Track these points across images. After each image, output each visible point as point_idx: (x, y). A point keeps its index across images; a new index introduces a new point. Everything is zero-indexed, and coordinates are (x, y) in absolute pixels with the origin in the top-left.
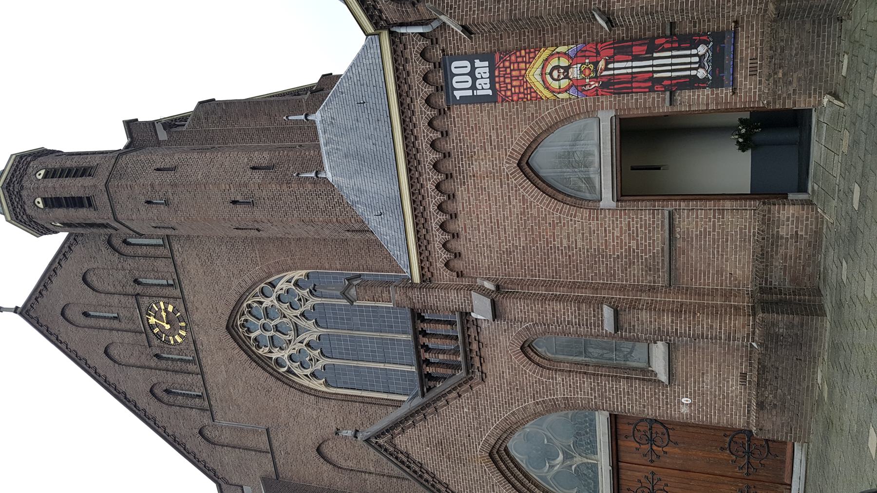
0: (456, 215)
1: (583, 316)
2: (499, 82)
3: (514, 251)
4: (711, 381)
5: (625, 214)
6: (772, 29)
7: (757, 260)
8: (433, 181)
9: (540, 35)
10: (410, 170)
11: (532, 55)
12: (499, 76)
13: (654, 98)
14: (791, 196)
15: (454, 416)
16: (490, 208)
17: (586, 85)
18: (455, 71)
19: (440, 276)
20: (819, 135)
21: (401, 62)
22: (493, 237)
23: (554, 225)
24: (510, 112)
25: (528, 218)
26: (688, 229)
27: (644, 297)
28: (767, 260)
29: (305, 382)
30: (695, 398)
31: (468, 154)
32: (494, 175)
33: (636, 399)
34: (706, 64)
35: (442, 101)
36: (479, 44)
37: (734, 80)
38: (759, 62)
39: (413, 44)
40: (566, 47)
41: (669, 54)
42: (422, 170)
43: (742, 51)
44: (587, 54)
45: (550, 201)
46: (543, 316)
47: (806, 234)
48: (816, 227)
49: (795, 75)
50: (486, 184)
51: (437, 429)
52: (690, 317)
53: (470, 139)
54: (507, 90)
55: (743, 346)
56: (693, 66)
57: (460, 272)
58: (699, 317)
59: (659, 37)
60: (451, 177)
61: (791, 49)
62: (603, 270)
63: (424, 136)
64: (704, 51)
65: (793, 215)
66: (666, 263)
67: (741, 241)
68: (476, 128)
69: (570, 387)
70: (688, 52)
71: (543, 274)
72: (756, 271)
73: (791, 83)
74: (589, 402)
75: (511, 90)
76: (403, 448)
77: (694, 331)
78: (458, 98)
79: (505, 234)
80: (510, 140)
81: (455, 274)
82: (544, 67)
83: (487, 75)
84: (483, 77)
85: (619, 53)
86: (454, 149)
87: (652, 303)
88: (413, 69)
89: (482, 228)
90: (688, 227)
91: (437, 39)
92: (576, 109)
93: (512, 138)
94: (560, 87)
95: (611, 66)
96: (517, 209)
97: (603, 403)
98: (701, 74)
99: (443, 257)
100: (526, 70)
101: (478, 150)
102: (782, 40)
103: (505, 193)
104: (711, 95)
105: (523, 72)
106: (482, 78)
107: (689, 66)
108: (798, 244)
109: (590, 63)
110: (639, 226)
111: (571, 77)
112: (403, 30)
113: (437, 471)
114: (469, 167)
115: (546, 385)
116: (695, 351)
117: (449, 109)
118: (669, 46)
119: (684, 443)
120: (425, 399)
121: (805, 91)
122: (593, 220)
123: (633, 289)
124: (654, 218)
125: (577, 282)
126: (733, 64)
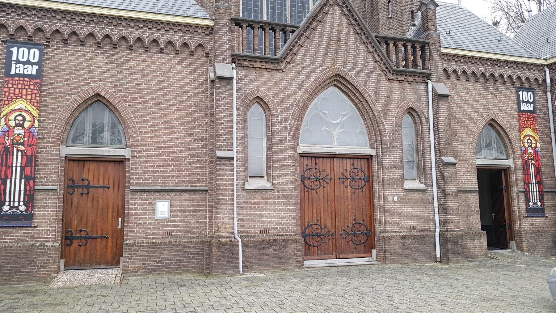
1: (446, 146)
4: (408, 212)
11: (35, 104)
12: (23, 80)
16: (472, 101)
17: (9, 137)
18: (32, 51)
25: (469, 121)
30: (398, 203)
33: (392, 171)
41: (537, 190)
42: (187, 34)
48: (479, 256)
49: (534, 241)
54: (13, 85)
55: (429, 227)
60: (485, 82)
64: (21, 209)
69: (393, 134)
70: (22, 199)
73: (531, 239)
74: (385, 144)
75: (12, 87)
77: (450, 203)
78: (11, 49)
82: (531, 136)
83: (26, 73)
89: (462, 94)
95: (20, 153)
97: (386, 152)
98: (531, 204)
100: (26, 99)
105: (24, 97)
106: (24, 69)
107: (12, 200)
109: (24, 140)
111: (16, 128)
115: (392, 119)
116: (424, 203)
117: (514, 87)
118: (28, 187)
119: (355, 198)
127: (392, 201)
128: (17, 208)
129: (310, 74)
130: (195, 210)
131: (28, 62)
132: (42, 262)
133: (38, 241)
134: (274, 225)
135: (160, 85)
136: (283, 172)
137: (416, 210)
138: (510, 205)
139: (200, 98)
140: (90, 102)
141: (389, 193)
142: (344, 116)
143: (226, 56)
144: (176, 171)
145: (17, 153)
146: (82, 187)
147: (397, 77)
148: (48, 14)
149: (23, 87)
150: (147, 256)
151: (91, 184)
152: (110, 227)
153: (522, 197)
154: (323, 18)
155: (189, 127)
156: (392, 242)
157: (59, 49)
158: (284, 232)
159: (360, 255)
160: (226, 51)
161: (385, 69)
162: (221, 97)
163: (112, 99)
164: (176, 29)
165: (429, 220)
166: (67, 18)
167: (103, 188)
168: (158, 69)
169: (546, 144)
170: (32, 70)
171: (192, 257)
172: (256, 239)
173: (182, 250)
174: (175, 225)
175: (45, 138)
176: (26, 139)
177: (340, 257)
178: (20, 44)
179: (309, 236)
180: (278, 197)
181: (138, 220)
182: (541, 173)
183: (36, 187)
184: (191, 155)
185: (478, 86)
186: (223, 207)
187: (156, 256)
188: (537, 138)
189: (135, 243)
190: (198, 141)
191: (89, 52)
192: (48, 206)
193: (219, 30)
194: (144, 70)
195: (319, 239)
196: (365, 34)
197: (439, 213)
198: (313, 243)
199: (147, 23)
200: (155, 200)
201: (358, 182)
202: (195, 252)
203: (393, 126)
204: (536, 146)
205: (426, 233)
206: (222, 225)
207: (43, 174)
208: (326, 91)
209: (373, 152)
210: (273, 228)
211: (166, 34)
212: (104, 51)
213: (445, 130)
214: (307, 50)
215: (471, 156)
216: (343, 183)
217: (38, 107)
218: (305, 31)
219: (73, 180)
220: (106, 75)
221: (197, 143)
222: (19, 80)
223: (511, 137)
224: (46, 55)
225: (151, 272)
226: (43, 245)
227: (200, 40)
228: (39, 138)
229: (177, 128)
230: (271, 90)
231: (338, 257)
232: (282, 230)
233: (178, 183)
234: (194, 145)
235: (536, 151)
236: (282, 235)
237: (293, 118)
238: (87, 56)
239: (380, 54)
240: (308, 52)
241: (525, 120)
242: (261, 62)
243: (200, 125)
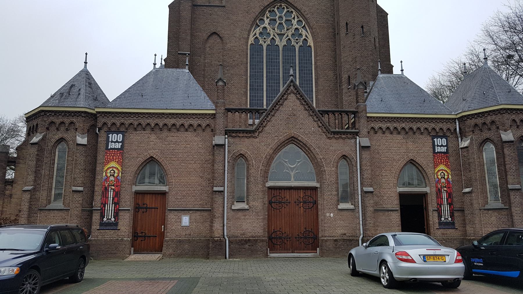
0: (392, 134)
1: (367, 180)
2: (112, 151)
3: (379, 155)
4: (341, 224)
10: (203, 115)
11: (120, 164)
12: (115, 152)
14: (133, 249)
15: (309, 123)
16: (395, 147)
18: (119, 135)
22: (384, 147)
23: (390, 170)
24: (430, 158)
25: (392, 161)
29: (252, 34)
32: (407, 150)
33: (330, 197)
37: (441, 229)
40: (121, 176)
41: (449, 209)
44: (448, 184)
46: (365, 165)
51: (301, 115)
54: (109, 154)
55: (356, 234)
59: (119, 206)
70: (113, 215)
75: (109, 156)
76: (289, 97)
78: (109, 135)
79: (386, 152)
83: (116, 147)
86: (416, 136)
88: (444, 125)
89: (387, 143)
91: (452, 134)
95: (112, 190)
97: (326, 185)
98: (443, 219)
100: (444, 164)
105: (443, 163)
106: (115, 145)
107: (108, 215)
113: (280, 112)
114: (410, 141)
116: (352, 218)
117: (430, 136)
120: (317, 112)
122: (393, 185)
124: (395, 205)
127: (329, 217)
128: (448, 219)
129: (274, 138)
130: (204, 221)
131: (117, 142)
132: (122, 248)
133: (120, 237)
134: (249, 231)
135: (185, 150)
136: (256, 198)
137: (347, 222)
138: (428, 220)
139: (208, 155)
140: (148, 161)
141: (327, 211)
142: (299, 162)
143: (222, 131)
144: (193, 199)
145: (111, 190)
146: (143, 208)
147: (334, 136)
148: (127, 115)
150: (176, 247)
151: (148, 207)
152: (157, 230)
153: (436, 214)
154: (284, 102)
155: (201, 173)
156: (328, 243)
157: (132, 133)
158: (255, 235)
159: (309, 251)
160: (222, 128)
161: (325, 131)
162: (217, 156)
163: (159, 159)
164: (194, 117)
165: (356, 229)
166: (136, 116)
167: (155, 208)
168: (184, 140)
169: (457, 175)
170: (118, 146)
171: (201, 248)
172: (237, 239)
173: (196, 244)
174: (192, 230)
175: (125, 182)
176: (115, 183)
177: (295, 252)
178: (113, 132)
179: (274, 238)
180: (252, 214)
181: (172, 227)
182: (452, 197)
183: (120, 209)
184: (202, 189)
185: (400, 137)
186: (217, 220)
187: (181, 247)
188: (449, 172)
189: (170, 240)
190: (206, 181)
191: (147, 134)
192: (125, 218)
193: (218, 116)
194: (177, 142)
195: (281, 240)
196: (311, 109)
197: (363, 225)
198: (277, 243)
200: (181, 215)
201: (308, 204)
202: (203, 245)
203: (331, 168)
204: (448, 177)
205: (353, 238)
206: (216, 230)
207: (123, 201)
208: (286, 147)
209: (318, 185)
210: (249, 232)
211: (189, 120)
212: (155, 132)
213: (366, 169)
214: (273, 123)
215: (393, 186)
216: (298, 205)
218: (271, 112)
219: (139, 204)
220: (156, 145)
221: (205, 182)
223: (427, 171)
224: (126, 137)
225: (178, 256)
226: (122, 240)
227: (208, 122)
228: (122, 182)
229: (195, 174)
230: (249, 149)
231: (293, 252)
232: (254, 234)
233: (194, 206)
234: (204, 183)
235: (448, 181)
236: (255, 237)
237: (263, 166)
238: (147, 136)
239: (322, 122)
240: (273, 124)
241: (439, 159)
242: (243, 133)
243: (208, 171)
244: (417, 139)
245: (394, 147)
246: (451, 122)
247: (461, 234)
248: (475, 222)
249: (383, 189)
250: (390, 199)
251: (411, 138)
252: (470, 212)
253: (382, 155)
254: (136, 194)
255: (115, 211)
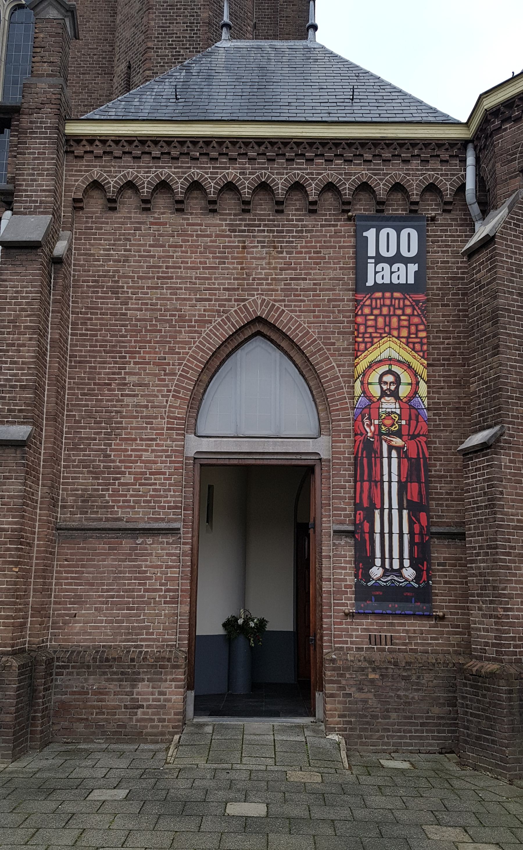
0: (180, 211)
2: (383, 298)
5: (176, 469)
6: (434, 665)
7: (97, 652)
8: (240, 179)
9: (444, 360)
11: (418, 347)
12: (392, 298)
13: (345, 509)
18: (404, 233)
19: (76, 171)
20: (284, 730)
21: (424, 153)
22: (142, 267)
23: (161, 364)
26: (151, 555)
27: (40, 491)
28: (99, 667)
31: (279, 242)
32: (244, 279)
34: (389, 578)
35: (360, 210)
36: (438, 273)
37: (365, 615)
38: (387, 647)
39: (447, 175)
41: (406, 530)
42: (259, 163)
43: (404, 625)
44: (413, 423)
45: (200, 362)
47: (138, 721)
49: (370, 695)
50: (231, 266)
52: (11, 556)
53: (302, 247)
54: (372, 309)
56: (387, 561)
57: (81, 205)
58: (11, 570)
59: (429, 517)
61: (406, 690)
62: (84, 433)
63: (312, 174)
64: (406, 576)
65: (169, 700)
66: (95, 523)
67: (128, 628)
68: (318, 258)
70: (406, 555)
71: (77, 340)
72: (79, 652)
73: (360, 690)
75: (371, 314)
78: (365, 234)
79: (148, 288)
80: (297, 309)
81: (80, 195)
83: (395, 281)
84: (393, 275)
85: (411, 466)
87: (32, 500)
89: (158, 252)
90: (154, 554)
91: (449, 211)
92: (337, 405)
93: (300, 311)
94: (371, 384)
95: (394, 453)
96: (189, 310)
98: (376, 572)
99: (110, 180)
100: (398, 338)
101: (285, 258)
102: (419, 677)
103: (215, 295)
104: (345, 585)
105: (395, 333)
106: (392, 273)
107: (387, 556)
108: (123, 710)
110: (158, 487)
111: (383, 400)
112: (470, 160)
114: (258, 242)
117: (349, 219)
121: (349, 709)
123: (54, 474)
125: (64, 393)
126: (387, 614)
128: (399, 572)
131: (398, 258)
145: (390, 453)
149: (391, 313)
199: (149, 146)
204: (415, 393)
215: (168, 429)
217: (424, 352)
222: (383, 298)
235: (412, 407)
244: (292, 231)
245: (186, 268)
246: (445, 156)
247: (459, 645)
248: (504, 589)
249: (121, 439)
250: (151, 485)
251: (264, 231)
252: (486, 540)
253: (131, 299)
254: (198, 467)
255: (417, 539)
